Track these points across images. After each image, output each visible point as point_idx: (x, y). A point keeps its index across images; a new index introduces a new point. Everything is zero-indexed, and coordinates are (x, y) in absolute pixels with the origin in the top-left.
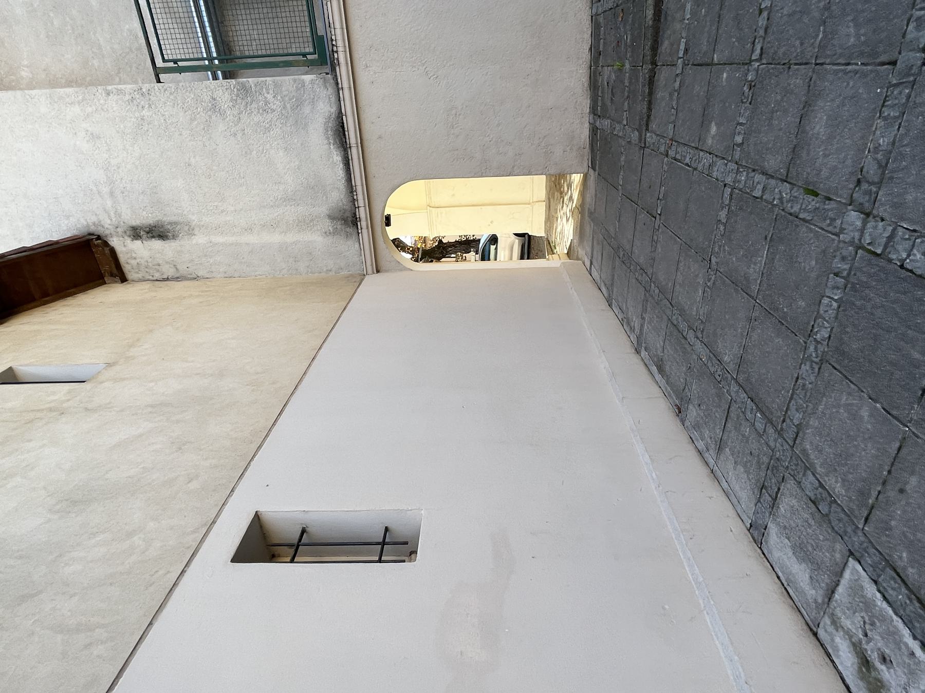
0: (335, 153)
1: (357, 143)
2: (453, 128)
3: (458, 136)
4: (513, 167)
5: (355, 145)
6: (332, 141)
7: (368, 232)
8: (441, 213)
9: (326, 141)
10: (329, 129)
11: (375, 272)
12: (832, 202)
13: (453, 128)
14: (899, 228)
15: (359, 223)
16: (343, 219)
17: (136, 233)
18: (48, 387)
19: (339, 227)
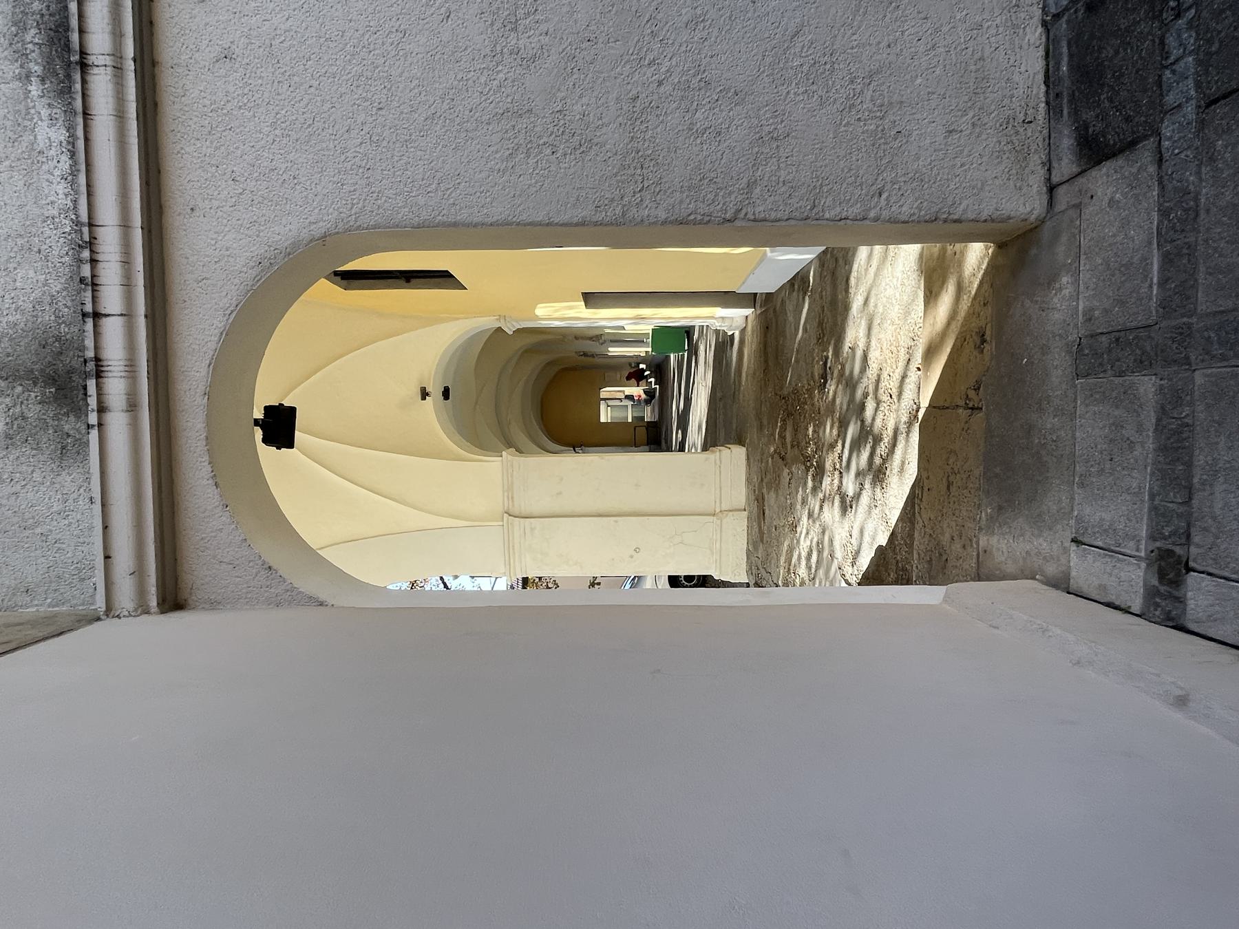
0: (45, 113)
1: (117, 55)
2: (515, 29)
3: (534, 58)
4: (751, 185)
5: (108, 60)
6: (37, 68)
7: (134, 426)
8: (532, 529)
9: (14, 69)
10: (31, 22)
11: (153, 603)
12: (851, 568)
13: (515, 29)
14: (494, 589)
15: (91, 384)
16: (52, 380)
17: (320, 549)
18: (676, 572)
19: (33, 411)
